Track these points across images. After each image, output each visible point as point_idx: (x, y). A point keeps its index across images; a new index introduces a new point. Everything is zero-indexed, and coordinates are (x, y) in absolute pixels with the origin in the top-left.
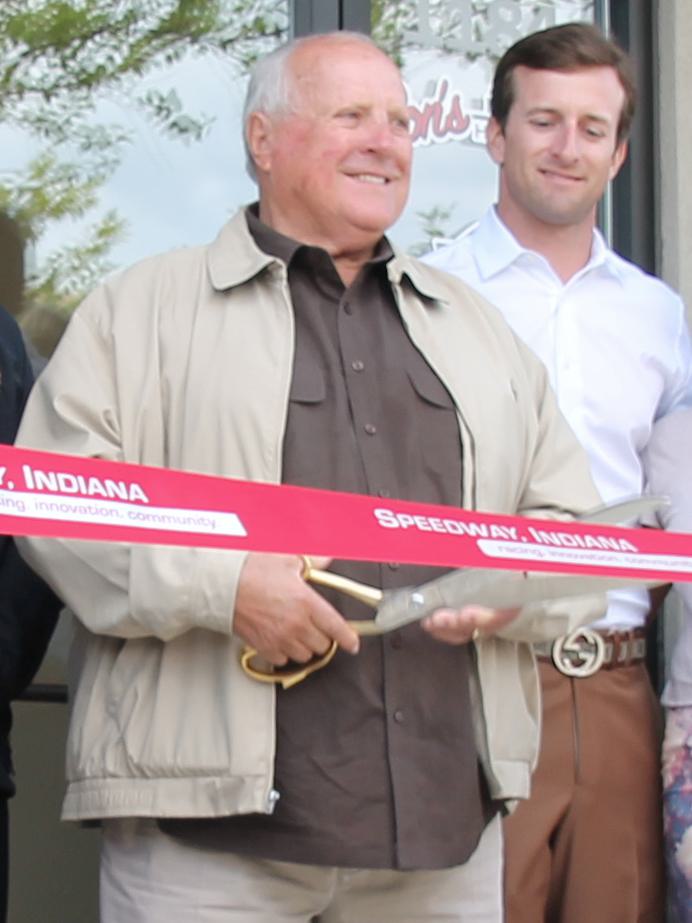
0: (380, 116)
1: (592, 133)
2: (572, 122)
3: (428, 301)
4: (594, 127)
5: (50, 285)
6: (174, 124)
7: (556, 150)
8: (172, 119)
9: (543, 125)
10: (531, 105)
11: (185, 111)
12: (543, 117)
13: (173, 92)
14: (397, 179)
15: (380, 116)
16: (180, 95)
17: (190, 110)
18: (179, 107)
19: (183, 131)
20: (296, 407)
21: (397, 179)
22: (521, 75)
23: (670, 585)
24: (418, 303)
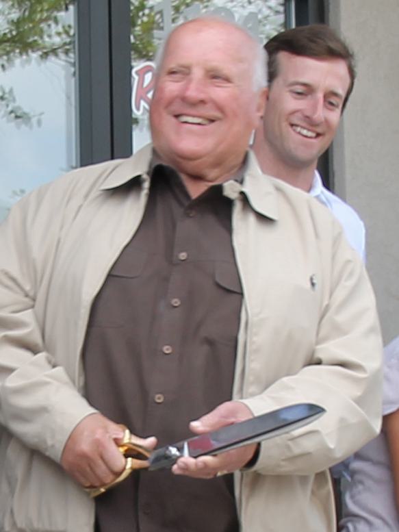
0: (198, 73)
1: (331, 104)
2: (320, 95)
3: (262, 218)
4: (334, 100)
5: (27, 54)
6: (12, 112)
7: (308, 114)
8: (10, 109)
9: (299, 93)
10: (292, 79)
11: (17, 104)
12: (300, 89)
13: (11, 91)
14: (219, 119)
15: (198, 73)
16: (15, 93)
17: (23, 102)
18: (14, 100)
19: (17, 117)
20: (238, 291)
21: (219, 119)
22: (283, 57)
23: (47, 383)
24: (252, 218)
